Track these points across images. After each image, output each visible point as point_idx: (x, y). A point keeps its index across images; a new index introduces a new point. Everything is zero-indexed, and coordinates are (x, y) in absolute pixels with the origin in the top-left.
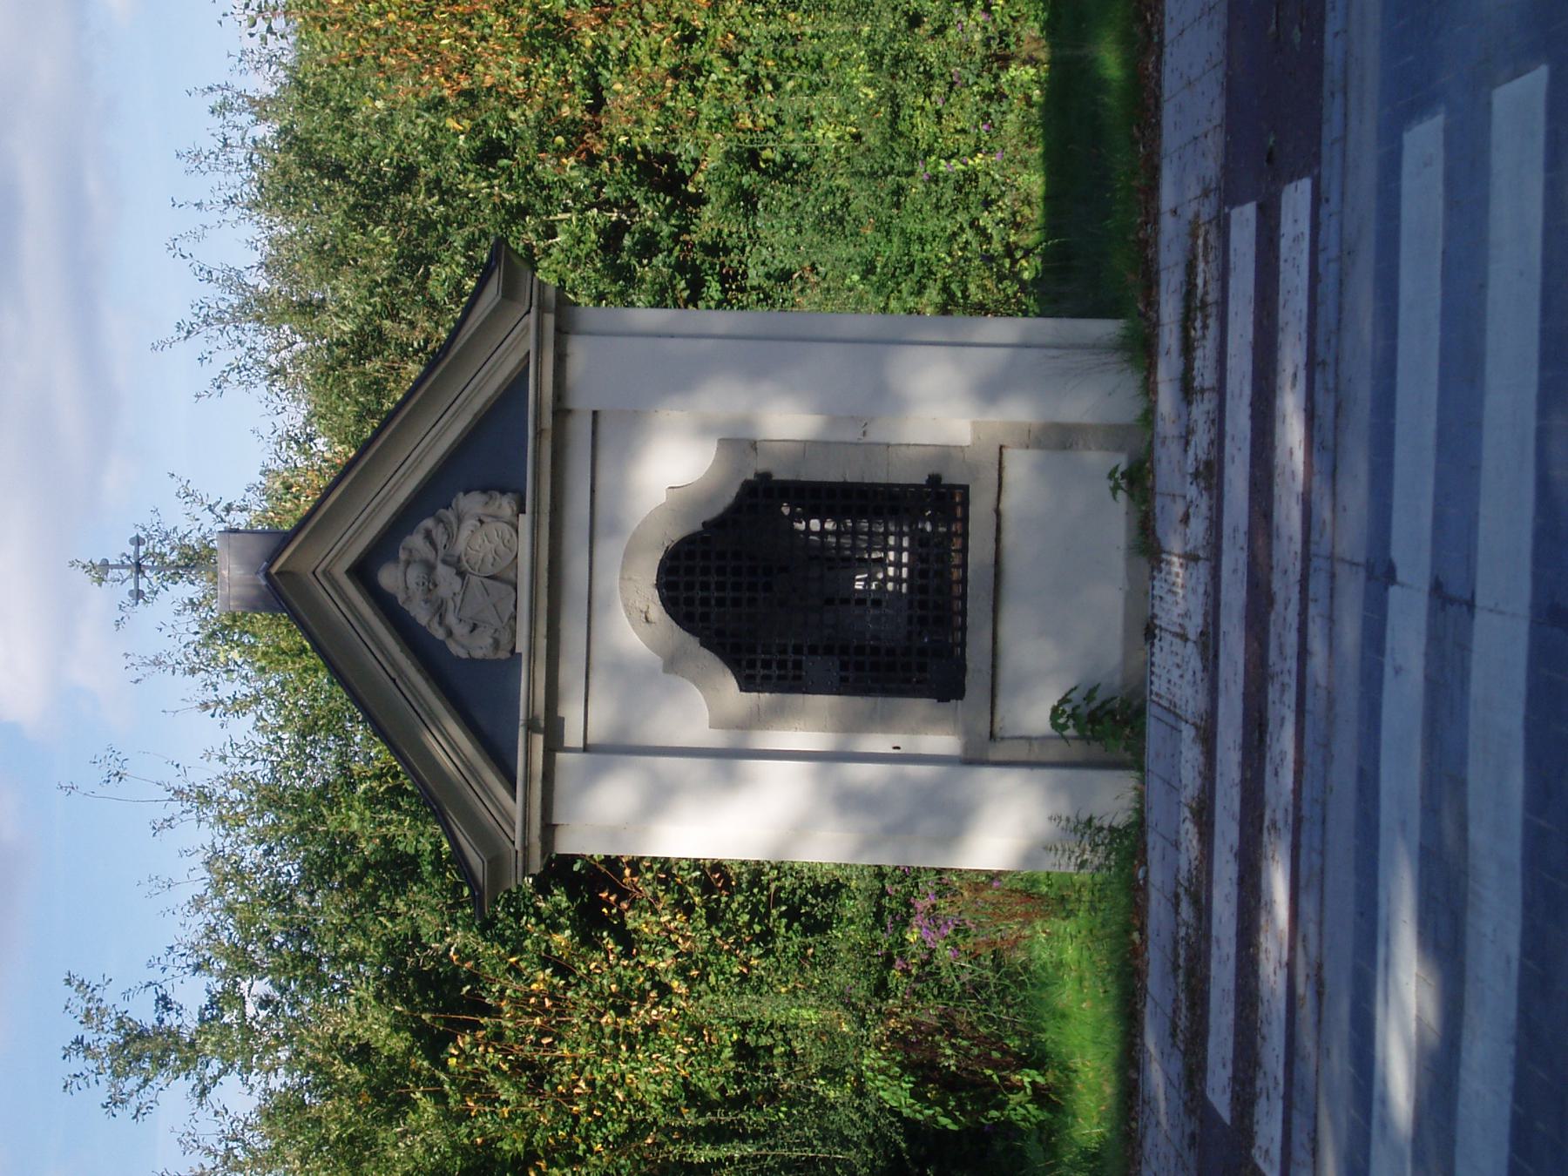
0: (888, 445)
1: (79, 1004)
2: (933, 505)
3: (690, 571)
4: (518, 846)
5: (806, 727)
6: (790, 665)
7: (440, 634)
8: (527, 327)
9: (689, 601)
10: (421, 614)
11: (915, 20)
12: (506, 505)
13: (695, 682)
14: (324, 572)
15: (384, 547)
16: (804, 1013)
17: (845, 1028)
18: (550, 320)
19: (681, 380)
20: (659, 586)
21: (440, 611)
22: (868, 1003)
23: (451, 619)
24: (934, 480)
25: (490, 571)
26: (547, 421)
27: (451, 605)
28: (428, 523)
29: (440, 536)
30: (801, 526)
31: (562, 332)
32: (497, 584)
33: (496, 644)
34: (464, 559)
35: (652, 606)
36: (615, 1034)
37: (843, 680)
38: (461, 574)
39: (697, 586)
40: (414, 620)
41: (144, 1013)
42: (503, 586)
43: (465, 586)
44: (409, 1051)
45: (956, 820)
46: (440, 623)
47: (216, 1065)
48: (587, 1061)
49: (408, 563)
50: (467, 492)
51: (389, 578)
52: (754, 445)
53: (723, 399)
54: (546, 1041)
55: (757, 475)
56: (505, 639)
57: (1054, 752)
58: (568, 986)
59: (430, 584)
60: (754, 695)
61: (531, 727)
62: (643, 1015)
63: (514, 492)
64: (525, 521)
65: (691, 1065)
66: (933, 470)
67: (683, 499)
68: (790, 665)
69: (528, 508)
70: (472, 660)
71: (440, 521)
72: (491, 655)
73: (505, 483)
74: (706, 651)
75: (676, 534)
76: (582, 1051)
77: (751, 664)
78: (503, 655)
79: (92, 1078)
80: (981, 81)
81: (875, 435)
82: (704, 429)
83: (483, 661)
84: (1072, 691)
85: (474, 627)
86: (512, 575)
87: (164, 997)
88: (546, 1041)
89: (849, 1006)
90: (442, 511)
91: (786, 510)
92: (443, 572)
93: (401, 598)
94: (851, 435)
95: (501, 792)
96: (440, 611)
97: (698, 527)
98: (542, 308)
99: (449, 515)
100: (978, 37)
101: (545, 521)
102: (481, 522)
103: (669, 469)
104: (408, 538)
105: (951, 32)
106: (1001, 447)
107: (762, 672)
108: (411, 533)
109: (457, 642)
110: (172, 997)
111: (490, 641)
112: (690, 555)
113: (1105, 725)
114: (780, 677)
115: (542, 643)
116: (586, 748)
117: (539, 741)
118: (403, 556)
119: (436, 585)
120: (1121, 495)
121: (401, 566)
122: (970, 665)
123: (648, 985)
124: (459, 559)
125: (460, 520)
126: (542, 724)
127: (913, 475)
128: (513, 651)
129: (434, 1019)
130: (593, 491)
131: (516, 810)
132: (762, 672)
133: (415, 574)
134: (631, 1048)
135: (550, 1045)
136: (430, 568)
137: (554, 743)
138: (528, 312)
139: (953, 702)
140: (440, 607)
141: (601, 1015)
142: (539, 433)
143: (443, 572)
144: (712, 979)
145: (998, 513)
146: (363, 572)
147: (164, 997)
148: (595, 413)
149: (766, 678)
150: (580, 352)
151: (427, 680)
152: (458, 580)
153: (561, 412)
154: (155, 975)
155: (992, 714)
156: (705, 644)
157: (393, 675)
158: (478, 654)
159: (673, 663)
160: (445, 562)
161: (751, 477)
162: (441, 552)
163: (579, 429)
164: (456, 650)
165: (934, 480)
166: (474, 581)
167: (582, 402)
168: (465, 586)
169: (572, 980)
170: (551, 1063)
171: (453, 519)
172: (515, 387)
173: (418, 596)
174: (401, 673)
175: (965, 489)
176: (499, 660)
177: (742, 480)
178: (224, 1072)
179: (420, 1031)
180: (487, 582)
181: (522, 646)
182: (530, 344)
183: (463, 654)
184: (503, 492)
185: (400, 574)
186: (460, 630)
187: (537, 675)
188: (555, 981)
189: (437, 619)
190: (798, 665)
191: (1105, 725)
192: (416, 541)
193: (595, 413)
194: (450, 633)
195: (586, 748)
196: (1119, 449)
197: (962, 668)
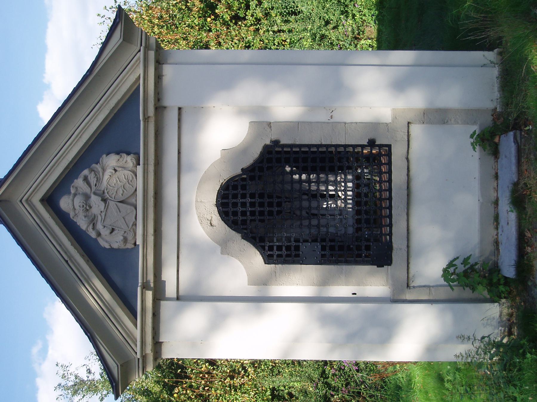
0: (345, 123)
1: (61, 372)
2: (368, 159)
3: (235, 196)
4: (139, 356)
5: (299, 280)
6: (293, 248)
7: (93, 235)
8: (139, 59)
9: (235, 214)
10: (82, 223)
11: (327, 23)
12: (129, 160)
13: (237, 257)
14: (27, 200)
15: (62, 185)
16: (295, 384)
17: (311, 389)
18: (152, 54)
19: (226, 84)
20: (217, 205)
21: (93, 222)
22: (319, 379)
23: (99, 226)
24: (372, 143)
25: (120, 197)
26: (151, 111)
27: (100, 218)
28: (86, 172)
29: (92, 179)
30: (296, 177)
31: (159, 63)
32: (124, 205)
33: (125, 240)
34: (106, 192)
35: (214, 216)
36: (230, 386)
37: (323, 256)
38: (104, 200)
39: (239, 205)
40: (79, 226)
41: (83, 375)
42: (129, 207)
43: (107, 208)
44: (161, 392)
45: (388, 332)
46: (94, 228)
47: (105, 392)
48: (221, 395)
49: (75, 195)
50: (108, 154)
51: (65, 203)
52: (269, 124)
53: (249, 92)
54: (206, 388)
55: (271, 141)
56: (130, 238)
57: (444, 293)
58: (214, 369)
59: (87, 207)
60: (273, 266)
61: (145, 287)
62: (237, 381)
63: (134, 154)
64: (140, 170)
65: (256, 397)
66: (371, 136)
67: (231, 155)
68: (293, 248)
69: (141, 162)
70: (112, 249)
71: (92, 170)
72: (122, 246)
73: (127, 148)
74: (245, 242)
75: (226, 176)
76: (218, 392)
77: (271, 248)
78: (130, 246)
79: (65, 396)
80: (351, 47)
81: (337, 118)
82: (241, 112)
83: (118, 250)
84: (455, 259)
85: (113, 230)
86: (133, 201)
87: (89, 369)
88: (206, 388)
89: (312, 380)
90: (94, 165)
91: (288, 169)
92: (95, 200)
93: (72, 215)
94: (322, 117)
95: (129, 323)
96: (93, 222)
97: (239, 172)
98: (147, 48)
99: (98, 167)
100: (350, 29)
101: (151, 168)
102: (115, 170)
103: (220, 135)
104: (75, 180)
105: (340, 27)
106: (409, 123)
107: (277, 253)
108: (77, 178)
109: (103, 239)
110: (91, 369)
111: (122, 238)
112: (235, 187)
113: (471, 279)
114: (287, 256)
115: (151, 239)
116: (178, 298)
117: (149, 295)
118: (73, 191)
119: (91, 207)
120: (478, 148)
121: (71, 197)
122: (395, 246)
123: (240, 370)
124: (104, 192)
125: (104, 170)
126: (152, 285)
127: (358, 138)
128: (135, 244)
129: (168, 381)
130: (179, 153)
131: (137, 333)
132: (277, 253)
133: (78, 201)
134: (236, 390)
135: (208, 390)
136: (87, 197)
137: (159, 295)
138: (140, 51)
139: (386, 267)
140: (93, 220)
141: (225, 380)
142: (146, 119)
143: (95, 200)
144: (262, 367)
145: (407, 159)
146: (50, 200)
147: (89, 369)
148: (180, 109)
149: (279, 256)
150: (168, 70)
151: (87, 262)
152: (103, 204)
153: (160, 109)
154: (87, 362)
155: (408, 273)
156: (245, 237)
157: (66, 258)
158: (115, 246)
159: (224, 246)
160: (95, 194)
161: (268, 142)
162: (93, 190)
163: (171, 118)
164: (103, 243)
165: (372, 143)
166: (112, 204)
167: (172, 100)
168: (107, 208)
169: (215, 367)
170: (209, 395)
171: (100, 170)
172: (133, 96)
173: (81, 215)
174: (71, 257)
175: (389, 146)
176: (128, 249)
177: (263, 145)
178: (108, 393)
179: (165, 385)
180: (120, 205)
181: (139, 242)
182: (141, 71)
183: (107, 246)
184: (128, 154)
185: (70, 201)
186: (105, 232)
187: (148, 257)
188: (209, 367)
189: (91, 226)
190: (297, 248)
191: (471, 279)
192: (79, 182)
193: (180, 109)
194: (99, 234)
195: (178, 298)
196: (475, 123)
197: (389, 247)
